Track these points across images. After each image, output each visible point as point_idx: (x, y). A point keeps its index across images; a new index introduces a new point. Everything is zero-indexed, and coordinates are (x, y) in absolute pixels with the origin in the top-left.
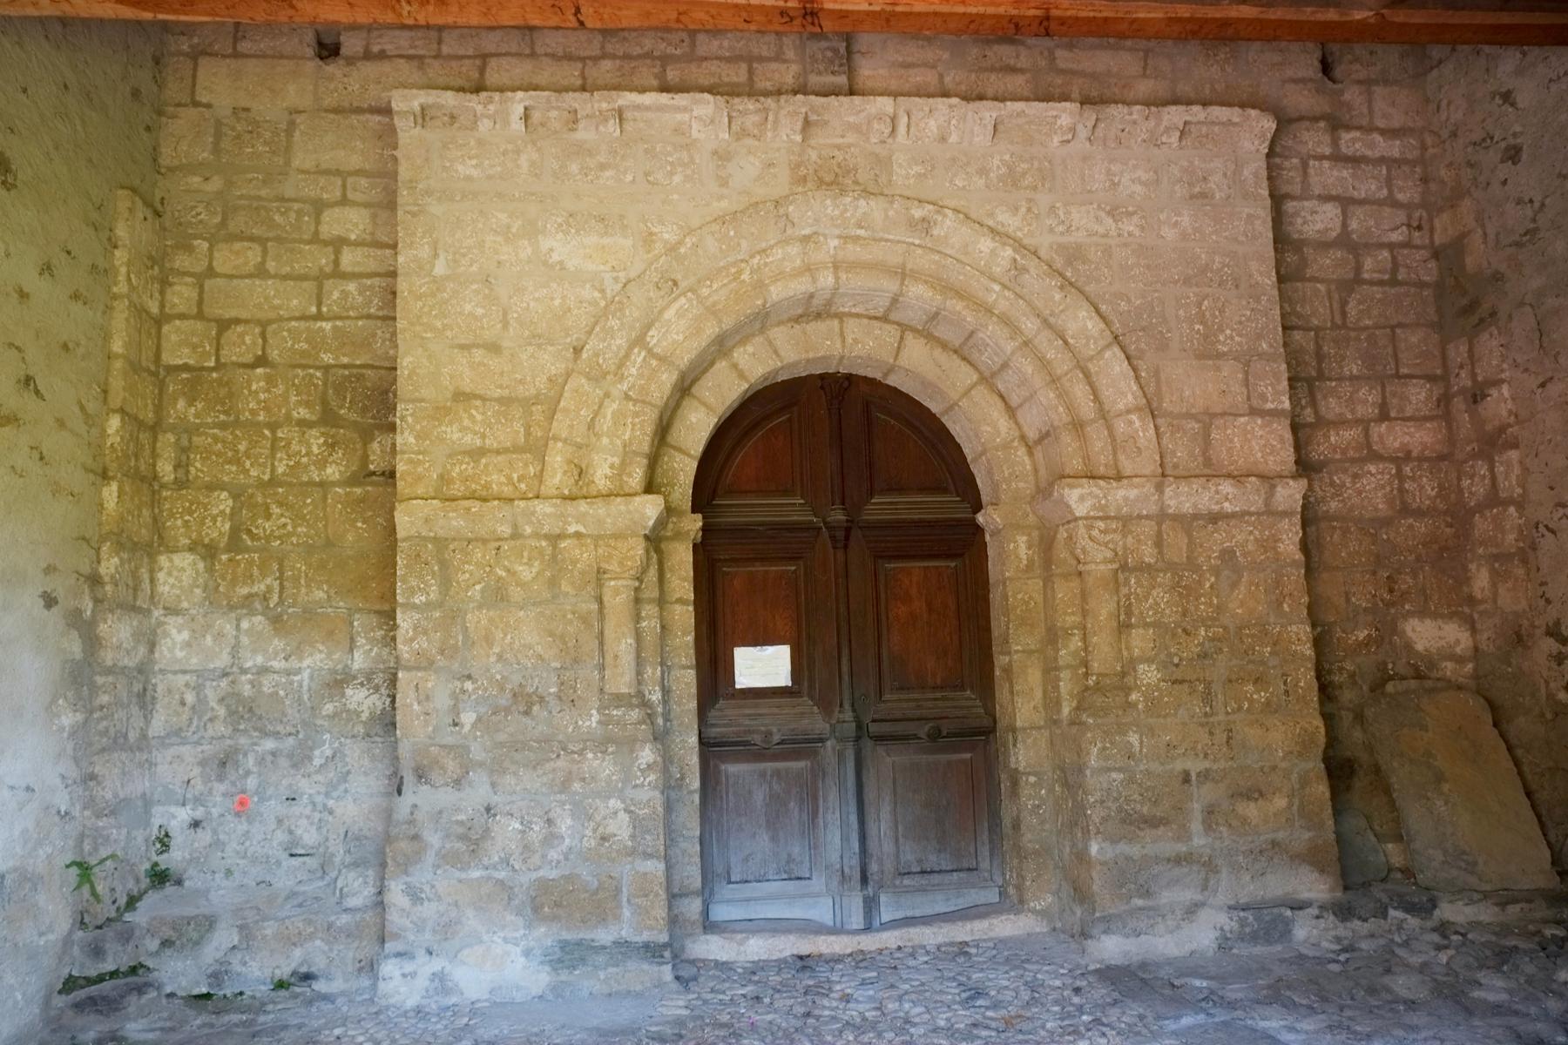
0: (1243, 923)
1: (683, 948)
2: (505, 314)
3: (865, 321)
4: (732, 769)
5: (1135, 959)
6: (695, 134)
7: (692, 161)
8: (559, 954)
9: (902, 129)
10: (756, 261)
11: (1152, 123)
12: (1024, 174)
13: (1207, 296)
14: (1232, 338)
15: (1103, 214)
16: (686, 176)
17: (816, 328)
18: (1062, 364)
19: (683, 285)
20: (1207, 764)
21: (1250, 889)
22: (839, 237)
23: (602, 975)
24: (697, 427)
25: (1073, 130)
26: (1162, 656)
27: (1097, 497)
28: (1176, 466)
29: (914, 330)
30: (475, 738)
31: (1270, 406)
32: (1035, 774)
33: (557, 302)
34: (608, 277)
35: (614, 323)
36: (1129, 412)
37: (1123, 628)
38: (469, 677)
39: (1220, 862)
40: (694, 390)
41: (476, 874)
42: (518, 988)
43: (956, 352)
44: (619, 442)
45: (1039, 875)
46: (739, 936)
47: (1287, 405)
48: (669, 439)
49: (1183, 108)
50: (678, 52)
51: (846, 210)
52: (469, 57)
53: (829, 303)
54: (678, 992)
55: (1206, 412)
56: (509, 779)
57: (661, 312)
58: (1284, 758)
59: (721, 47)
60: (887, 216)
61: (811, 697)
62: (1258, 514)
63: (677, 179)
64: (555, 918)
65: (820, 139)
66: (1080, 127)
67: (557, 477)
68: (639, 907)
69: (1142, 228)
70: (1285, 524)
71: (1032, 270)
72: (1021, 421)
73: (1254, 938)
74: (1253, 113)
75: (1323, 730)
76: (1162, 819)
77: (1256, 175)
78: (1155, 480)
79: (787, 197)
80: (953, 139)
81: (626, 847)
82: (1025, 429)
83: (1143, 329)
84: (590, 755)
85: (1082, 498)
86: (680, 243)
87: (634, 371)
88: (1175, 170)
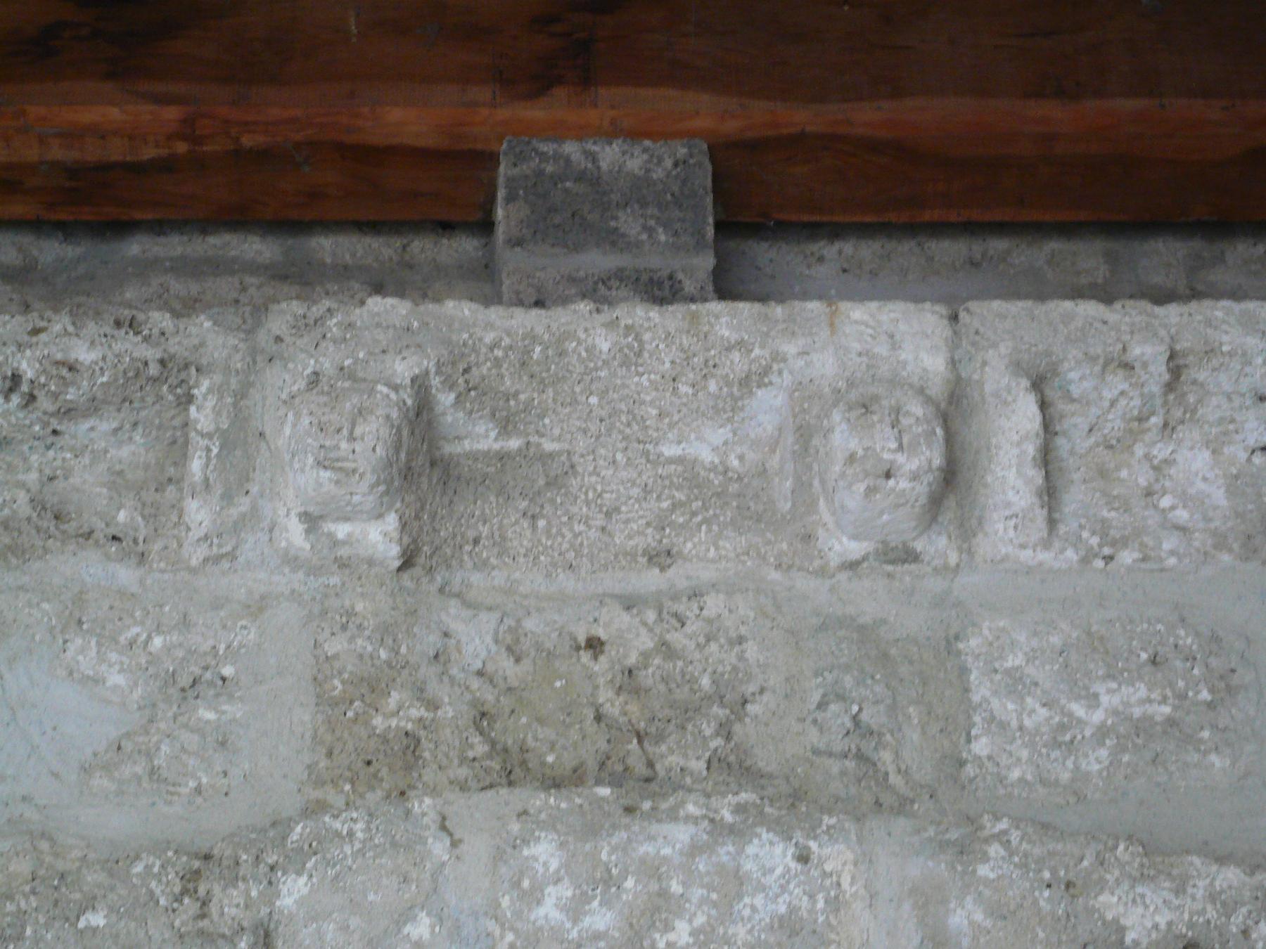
9: (1009, 478)
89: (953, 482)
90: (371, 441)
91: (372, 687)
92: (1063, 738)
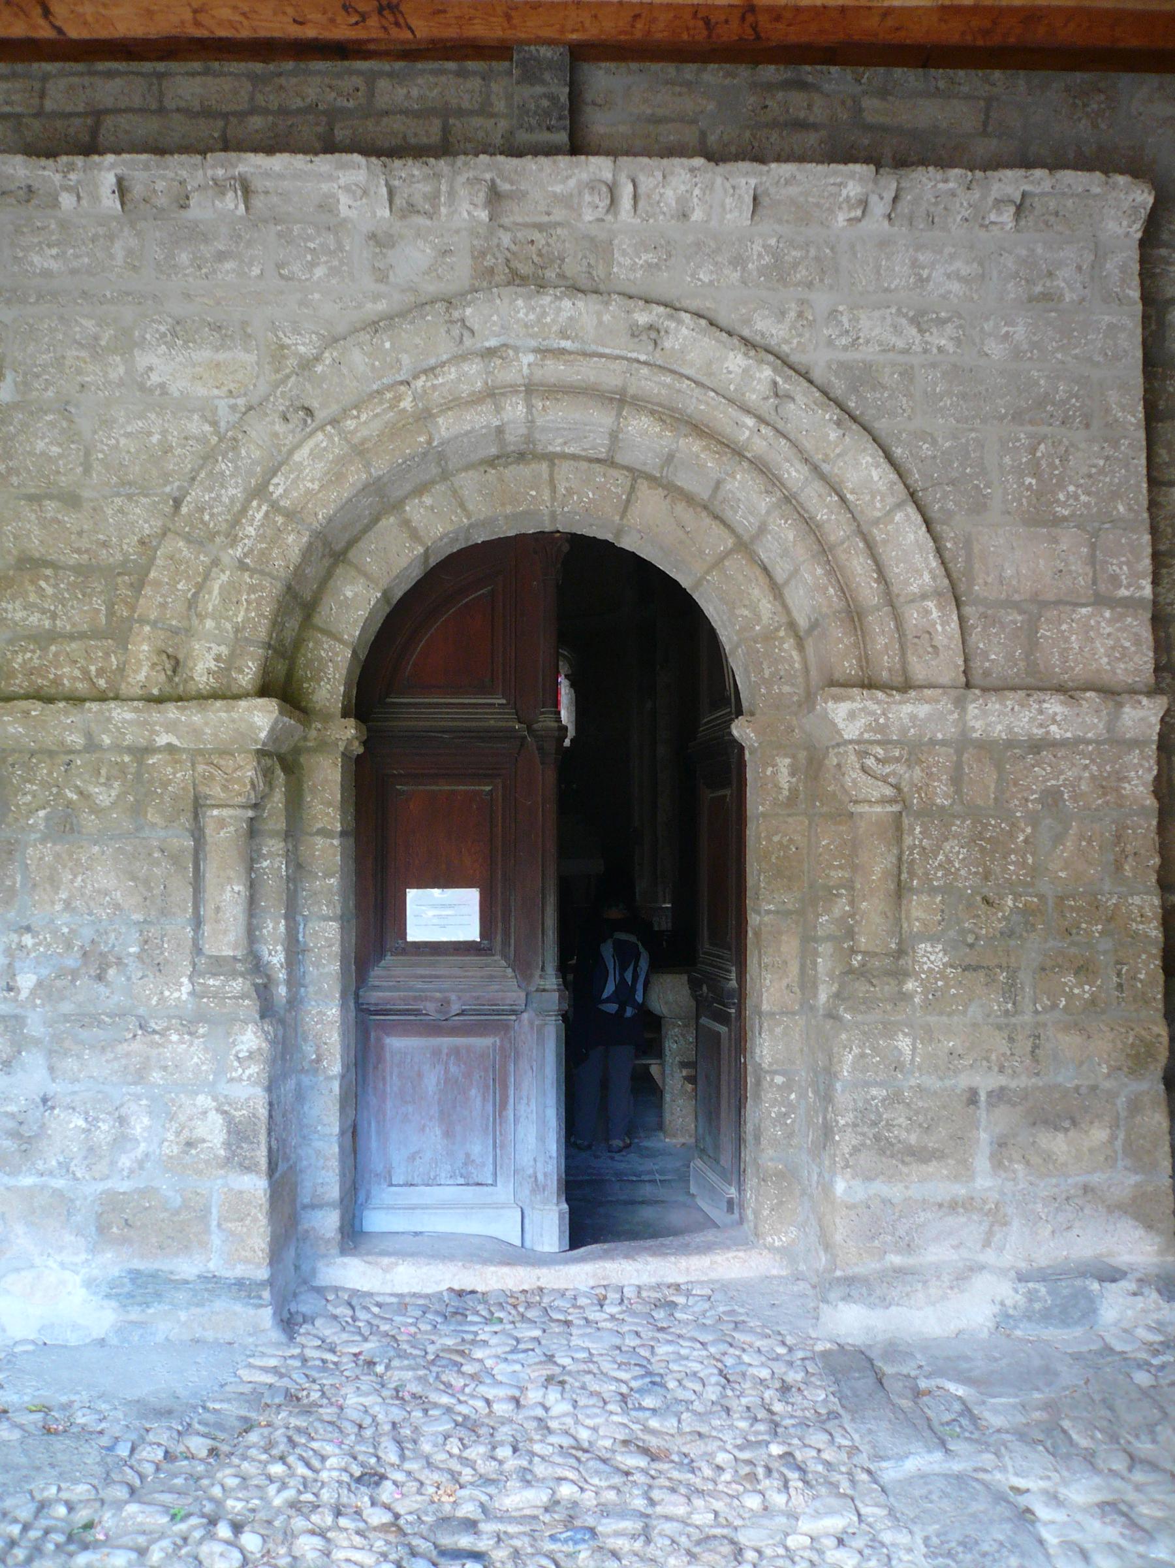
0: (1031, 1297)
1: (314, 1272)
2: (87, 454)
3: (584, 465)
4: (396, 1043)
5: (880, 1338)
6: (344, 211)
7: (340, 248)
8: (129, 1287)
9: (626, 202)
10: (419, 383)
11: (976, 194)
12: (795, 265)
13: (1043, 439)
14: (1076, 497)
15: (904, 321)
16: (330, 268)
17: (515, 473)
18: (837, 527)
19: (321, 415)
20: (1002, 1080)
21: (1050, 1249)
22: (536, 351)
23: (183, 1316)
24: (354, 606)
25: (864, 204)
26: (952, 934)
27: (873, 713)
28: (987, 673)
29: (650, 478)
30: (35, 1006)
31: (1123, 592)
32: (783, 1073)
33: (155, 439)
34: (223, 405)
35: (224, 466)
36: (924, 597)
37: (900, 892)
38: (28, 929)
39: (1010, 1210)
40: (351, 555)
41: (28, 1181)
42: (75, 1327)
43: (705, 508)
44: (228, 626)
45: (781, 1203)
46: (386, 1261)
47: (1148, 591)
48: (317, 620)
49: (1021, 172)
50: (351, 104)
51: (544, 314)
52: (78, 115)
53: (529, 439)
54: (278, 1345)
55: (1035, 599)
56: (70, 1063)
57: (291, 453)
58: (1109, 1076)
59: (408, 96)
60: (600, 323)
61: (505, 956)
62: (1098, 743)
63: (319, 272)
64: (124, 1241)
65: (515, 214)
66: (874, 199)
67: (143, 673)
68: (232, 1233)
69: (958, 342)
70: (1134, 757)
71: (798, 397)
72: (789, 602)
73: (1046, 1317)
74: (1121, 180)
75: (1165, 1040)
76: (935, 1151)
77: (1123, 269)
78: (954, 693)
79: (463, 295)
80: (697, 215)
81: (216, 1157)
82: (795, 614)
83: (952, 482)
84: (175, 1037)
85: (852, 716)
86: (317, 359)
87: (251, 531)
88: (1010, 262)
89: (613, 202)
90: (481, 197)
91: (483, 254)
92: (633, 268)
